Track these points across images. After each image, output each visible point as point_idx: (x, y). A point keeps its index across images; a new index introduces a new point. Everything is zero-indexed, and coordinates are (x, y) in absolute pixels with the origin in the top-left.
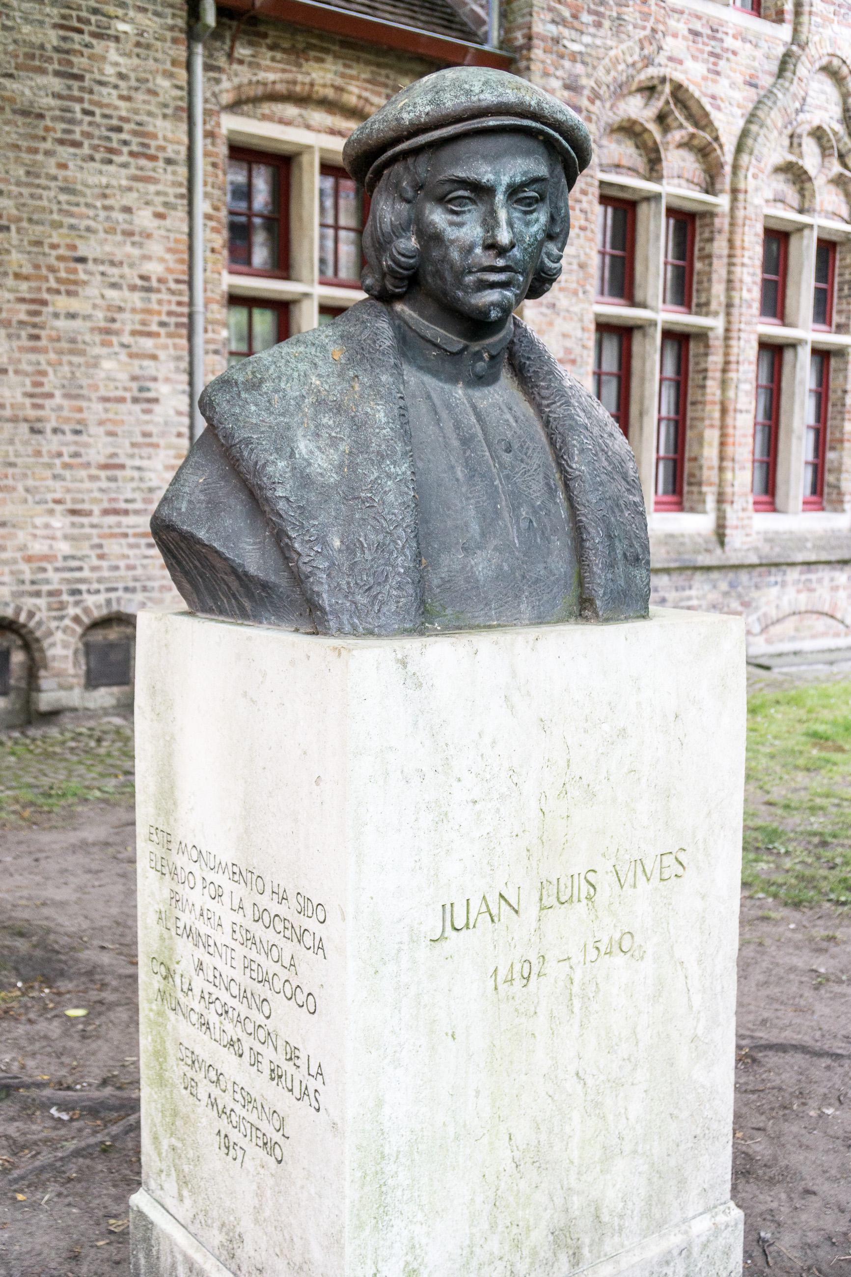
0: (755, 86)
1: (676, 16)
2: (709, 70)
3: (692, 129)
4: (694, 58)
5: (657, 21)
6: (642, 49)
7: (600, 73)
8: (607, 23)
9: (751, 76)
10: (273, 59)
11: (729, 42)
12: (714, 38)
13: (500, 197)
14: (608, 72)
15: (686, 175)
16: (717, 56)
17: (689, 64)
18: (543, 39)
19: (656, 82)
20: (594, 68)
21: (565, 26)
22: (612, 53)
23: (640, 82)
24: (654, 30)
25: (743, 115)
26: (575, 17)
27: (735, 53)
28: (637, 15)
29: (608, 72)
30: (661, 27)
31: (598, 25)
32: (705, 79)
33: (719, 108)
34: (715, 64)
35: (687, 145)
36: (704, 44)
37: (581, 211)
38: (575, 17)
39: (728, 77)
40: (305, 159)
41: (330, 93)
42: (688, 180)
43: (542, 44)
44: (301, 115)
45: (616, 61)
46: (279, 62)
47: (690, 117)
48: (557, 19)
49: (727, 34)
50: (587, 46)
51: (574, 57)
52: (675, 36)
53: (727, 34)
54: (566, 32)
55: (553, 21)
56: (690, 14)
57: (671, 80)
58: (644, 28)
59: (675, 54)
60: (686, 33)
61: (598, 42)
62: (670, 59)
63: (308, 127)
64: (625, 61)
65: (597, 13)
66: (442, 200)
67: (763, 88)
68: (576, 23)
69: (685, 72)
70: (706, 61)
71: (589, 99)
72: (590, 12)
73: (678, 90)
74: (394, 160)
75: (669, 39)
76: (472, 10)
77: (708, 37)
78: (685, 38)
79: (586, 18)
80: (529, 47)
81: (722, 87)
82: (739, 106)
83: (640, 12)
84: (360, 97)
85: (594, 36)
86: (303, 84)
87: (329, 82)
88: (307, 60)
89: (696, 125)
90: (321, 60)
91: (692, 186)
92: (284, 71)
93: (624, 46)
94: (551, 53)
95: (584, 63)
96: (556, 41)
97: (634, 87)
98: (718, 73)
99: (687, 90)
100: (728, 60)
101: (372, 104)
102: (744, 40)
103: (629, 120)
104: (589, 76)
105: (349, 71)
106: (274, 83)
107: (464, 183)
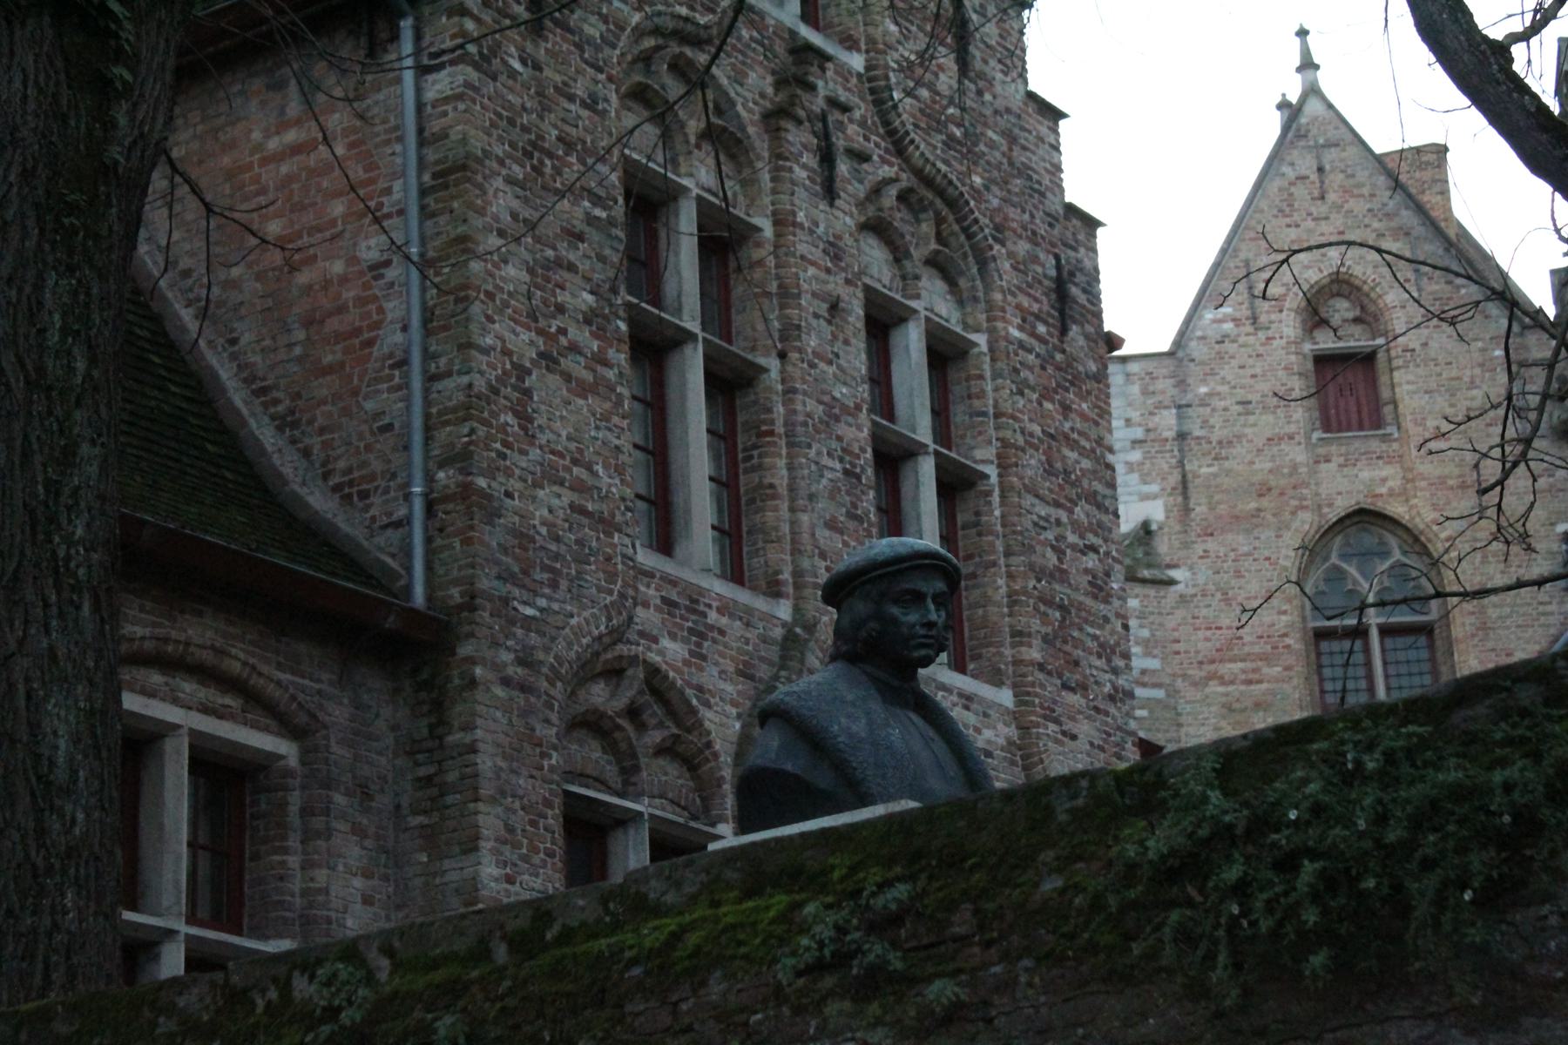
0: (751, 678)
1: (646, 580)
2: (691, 653)
3: (675, 731)
4: (673, 636)
5: (625, 585)
6: (609, 619)
7: (561, 645)
8: (564, 584)
9: (745, 663)
10: (142, 609)
11: (713, 616)
12: (695, 611)
13: (929, 600)
14: (570, 644)
15: (670, 795)
16: (702, 636)
17: (666, 643)
18: (490, 599)
19: (624, 664)
20: (553, 639)
21: (514, 584)
22: (574, 621)
23: (607, 661)
24: (622, 596)
25: (739, 716)
26: (525, 572)
27: (722, 632)
28: (601, 575)
29: (570, 644)
30: (631, 592)
31: (554, 585)
32: (686, 663)
33: (708, 705)
34: (699, 645)
35: (665, 750)
36: (682, 617)
37: (546, 829)
38: (525, 572)
39: (716, 664)
40: (169, 745)
41: (207, 657)
42: (672, 802)
43: (488, 605)
44: (167, 684)
45: (579, 632)
46: (148, 613)
47: (671, 713)
48: (505, 575)
49: (710, 606)
50: (542, 610)
51: (528, 622)
52: (646, 605)
53: (710, 606)
54: (516, 592)
55: (499, 577)
56: (661, 578)
57: (645, 661)
58: (610, 592)
59: (647, 628)
60: (658, 601)
61: (556, 606)
62: (642, 634)
63: (175, 701)
64: (590, 633)
65: (551, 570)
66: (896, 602)
67: (761, 680)
68: (527, 581)
69: (661, 653)
70: (685, 641)
71: (547, 679)
72: (545, 568)
73: (653, 672)
74: (863, 583)
75: (639, 609)
76: (378, 560)
77: (688, 609)
78: (658, 609)
79: (540, 575)
80: (473, 608)
81: (709, 677)
82: (734, 704)
83: (605, 572)
84: (245, 664)
85: (550, 599)
86: (177, 642)
87: (209, 643)
88: (182, 612)
89: (678, 725)
90: (200, 614)
91: (678, 810)
92: (154, 625)
93: (586, 614)
94: (499, 616)
95: (538, 632)
96: (506, 601)
97: (599, 668)
98: (704, 658)
99: (666, 677)
100: (714, 641)
101: (260, 674)
102: (732, 616)
103: (596, 711)
104: (547, 650)
105: (231, 630)
106: (143, 638)
107: (908, 591)
